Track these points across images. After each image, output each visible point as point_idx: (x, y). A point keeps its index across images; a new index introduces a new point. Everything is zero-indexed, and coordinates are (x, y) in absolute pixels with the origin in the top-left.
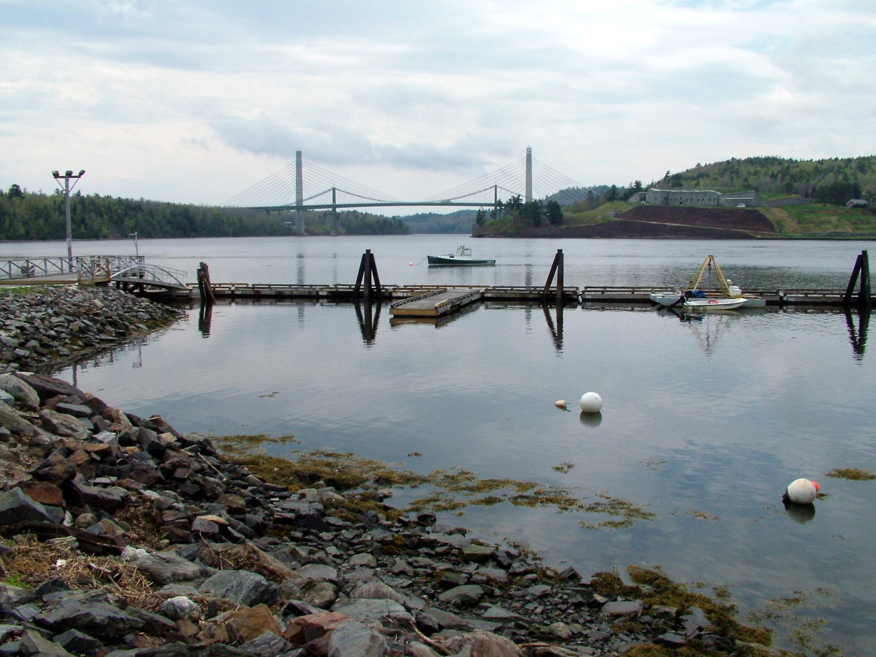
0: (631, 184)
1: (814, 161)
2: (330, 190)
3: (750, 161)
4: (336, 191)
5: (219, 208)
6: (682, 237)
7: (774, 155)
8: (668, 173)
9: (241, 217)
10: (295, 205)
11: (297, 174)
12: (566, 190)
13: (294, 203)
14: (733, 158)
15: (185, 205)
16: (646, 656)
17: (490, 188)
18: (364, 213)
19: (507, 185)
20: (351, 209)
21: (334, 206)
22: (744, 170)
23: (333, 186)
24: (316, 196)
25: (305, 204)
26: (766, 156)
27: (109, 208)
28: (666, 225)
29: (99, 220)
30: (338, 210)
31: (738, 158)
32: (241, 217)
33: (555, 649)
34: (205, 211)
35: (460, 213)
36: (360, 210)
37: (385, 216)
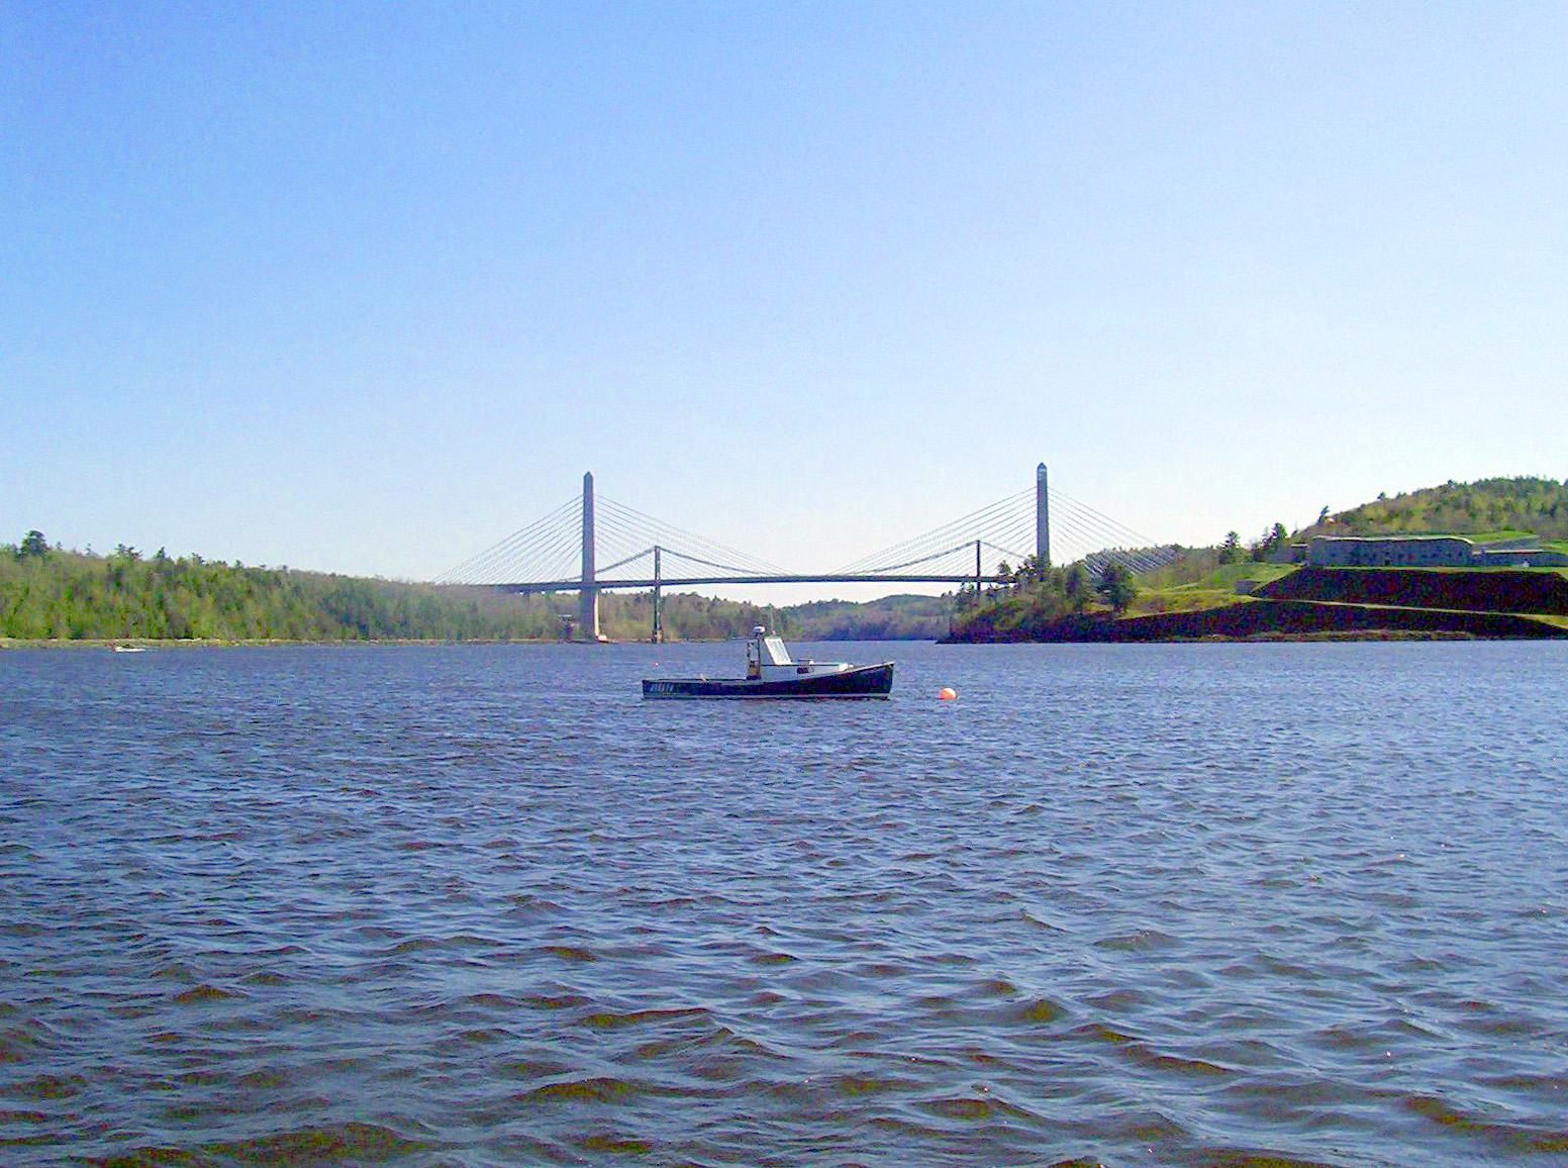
0: (1266, 529)
1: (1289, 533)
2: (650, 551)
3: (1483, 486)
4: (662, 553)
5: (431, 586)
6: (1175, 638)
7: (1533, 474)
8: (1325, 511)
9: (474, 603)
10: (580, 580)
11: (584, 520)
12: (1100, 553)
13: (579, 577)
14: (1450, 481)
15: (367, 579)
16: (1127, 1166)
17: (968, 545)
18: (712, 598)
19: (998, 541)
20: (687, 589)
21: (657, 583)
22: (1480, 502)
23: (656, 544)
24: (621, 564)
25: (598, 578)
26: (1518, 475)
27: (214, 579)
28: (1342, 599)
29: (196, 603)
30: (664, 591)
31: (1459, 480)
32: (474, 603)
33: (863, 1159)
34: (401, 591)
35: (888, 603)
36: (706, 591)
37: (754, 604)
